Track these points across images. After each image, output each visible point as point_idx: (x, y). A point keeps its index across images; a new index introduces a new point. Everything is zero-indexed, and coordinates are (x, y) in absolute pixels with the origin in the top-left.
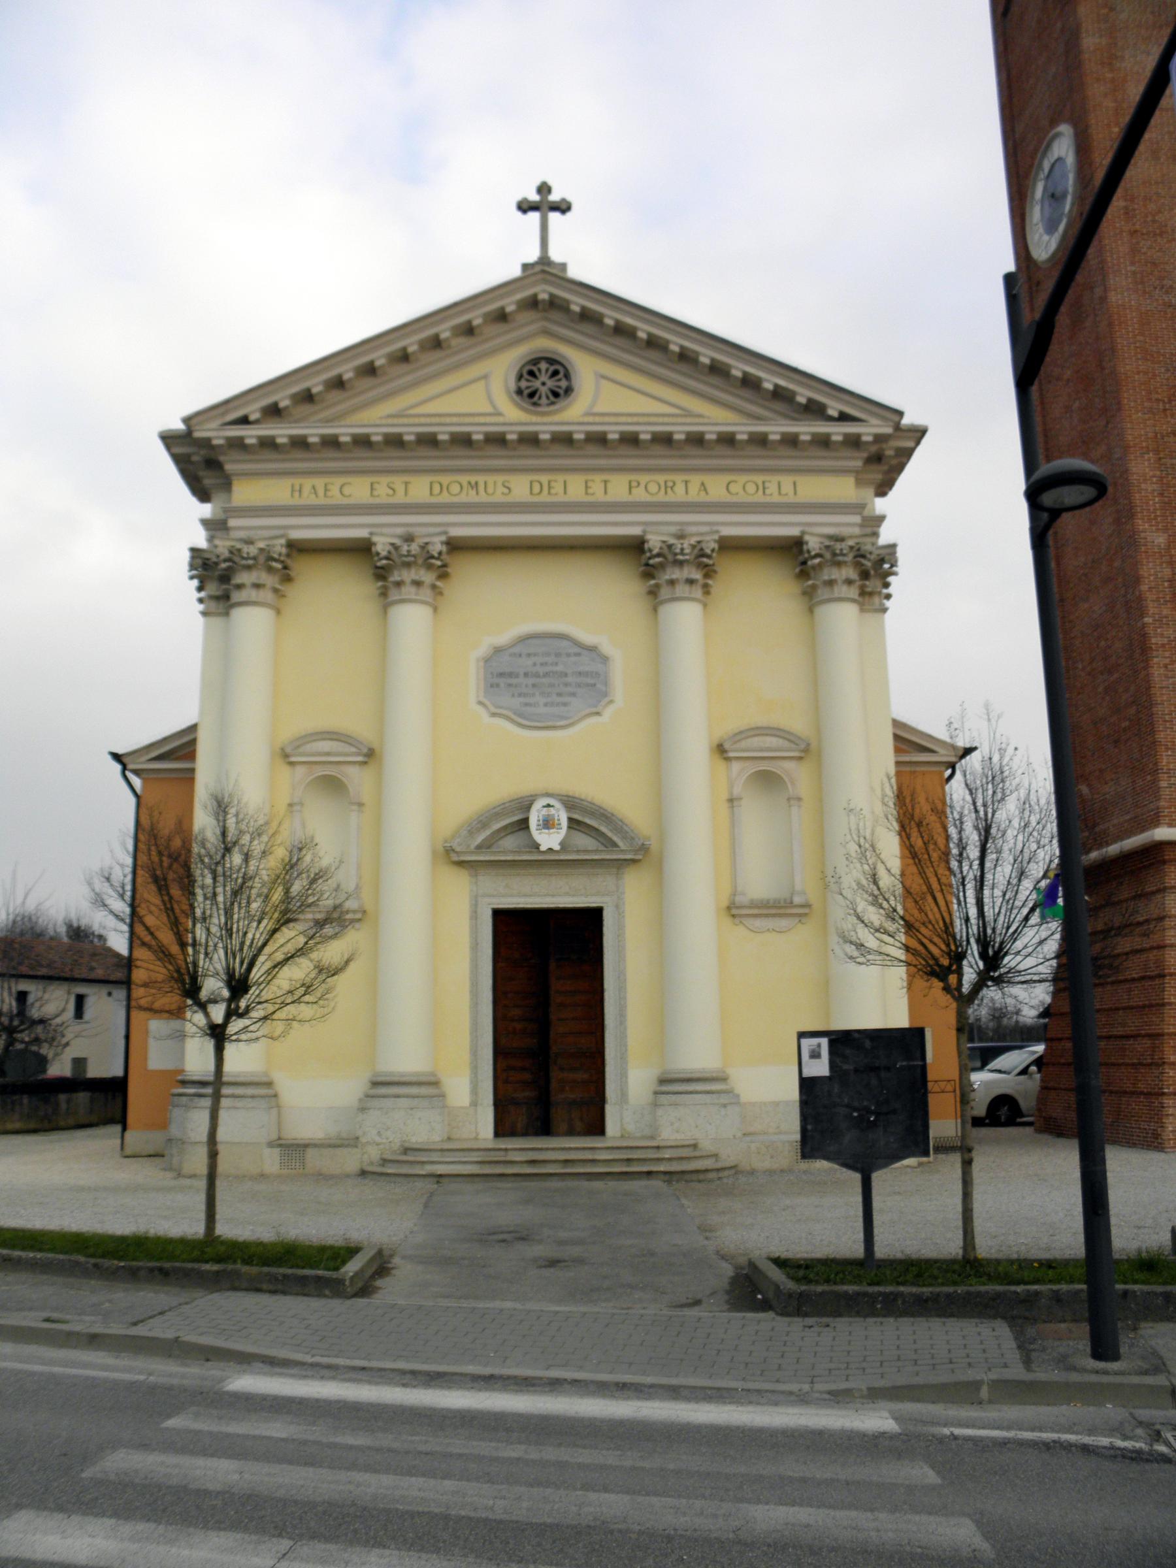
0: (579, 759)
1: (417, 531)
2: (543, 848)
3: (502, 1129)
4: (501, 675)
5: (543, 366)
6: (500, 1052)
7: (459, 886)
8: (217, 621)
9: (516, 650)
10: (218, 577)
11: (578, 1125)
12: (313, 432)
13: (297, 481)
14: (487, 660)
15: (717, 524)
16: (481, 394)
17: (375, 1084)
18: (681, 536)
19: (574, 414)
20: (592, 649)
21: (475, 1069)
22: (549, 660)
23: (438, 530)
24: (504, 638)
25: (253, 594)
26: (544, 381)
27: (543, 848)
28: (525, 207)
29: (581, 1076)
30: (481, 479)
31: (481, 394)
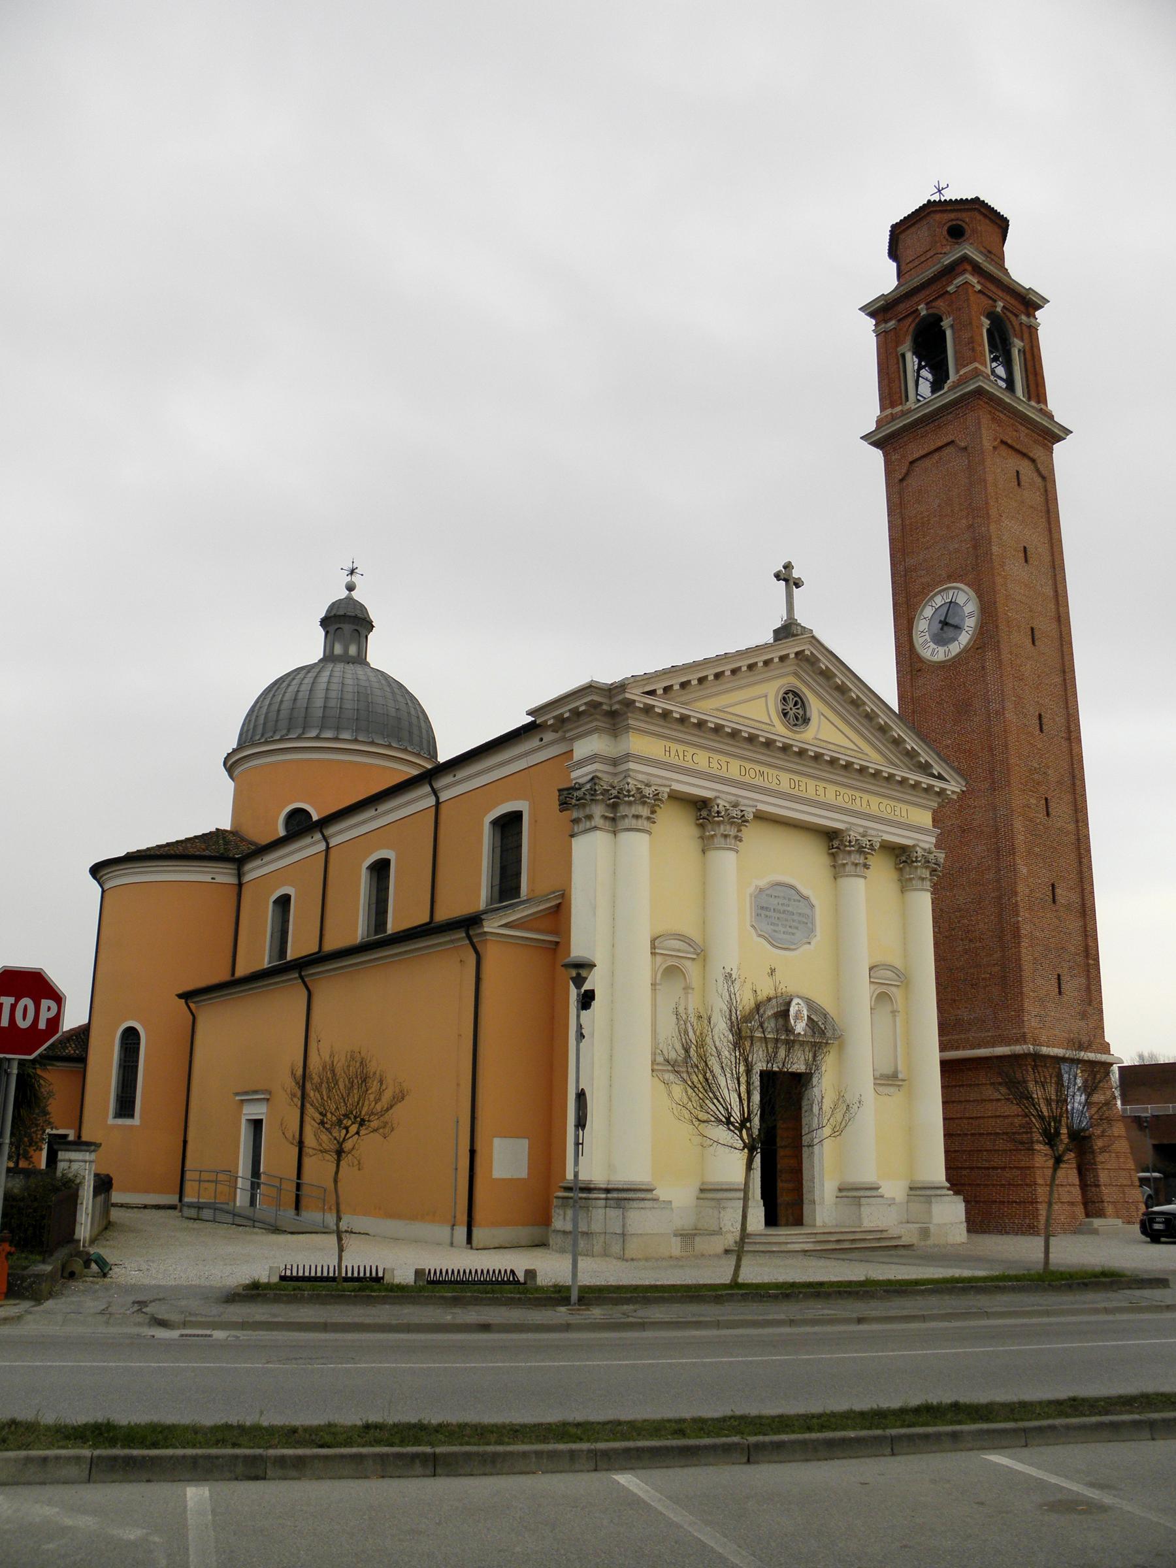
0: (799, 976)
1: (870, 832)
4: (762, 908)
5: (790, 695)
9: (768, 892)
12: (677, 711)
13: (668, 744)
15: (757, 801)
16: (756, 707)
20: (806, 898)
22: (786, 902)
23: (751, 803)
24: (763, 883)
25: (634, 823)
26: (794, 709)
31: (756, 707)
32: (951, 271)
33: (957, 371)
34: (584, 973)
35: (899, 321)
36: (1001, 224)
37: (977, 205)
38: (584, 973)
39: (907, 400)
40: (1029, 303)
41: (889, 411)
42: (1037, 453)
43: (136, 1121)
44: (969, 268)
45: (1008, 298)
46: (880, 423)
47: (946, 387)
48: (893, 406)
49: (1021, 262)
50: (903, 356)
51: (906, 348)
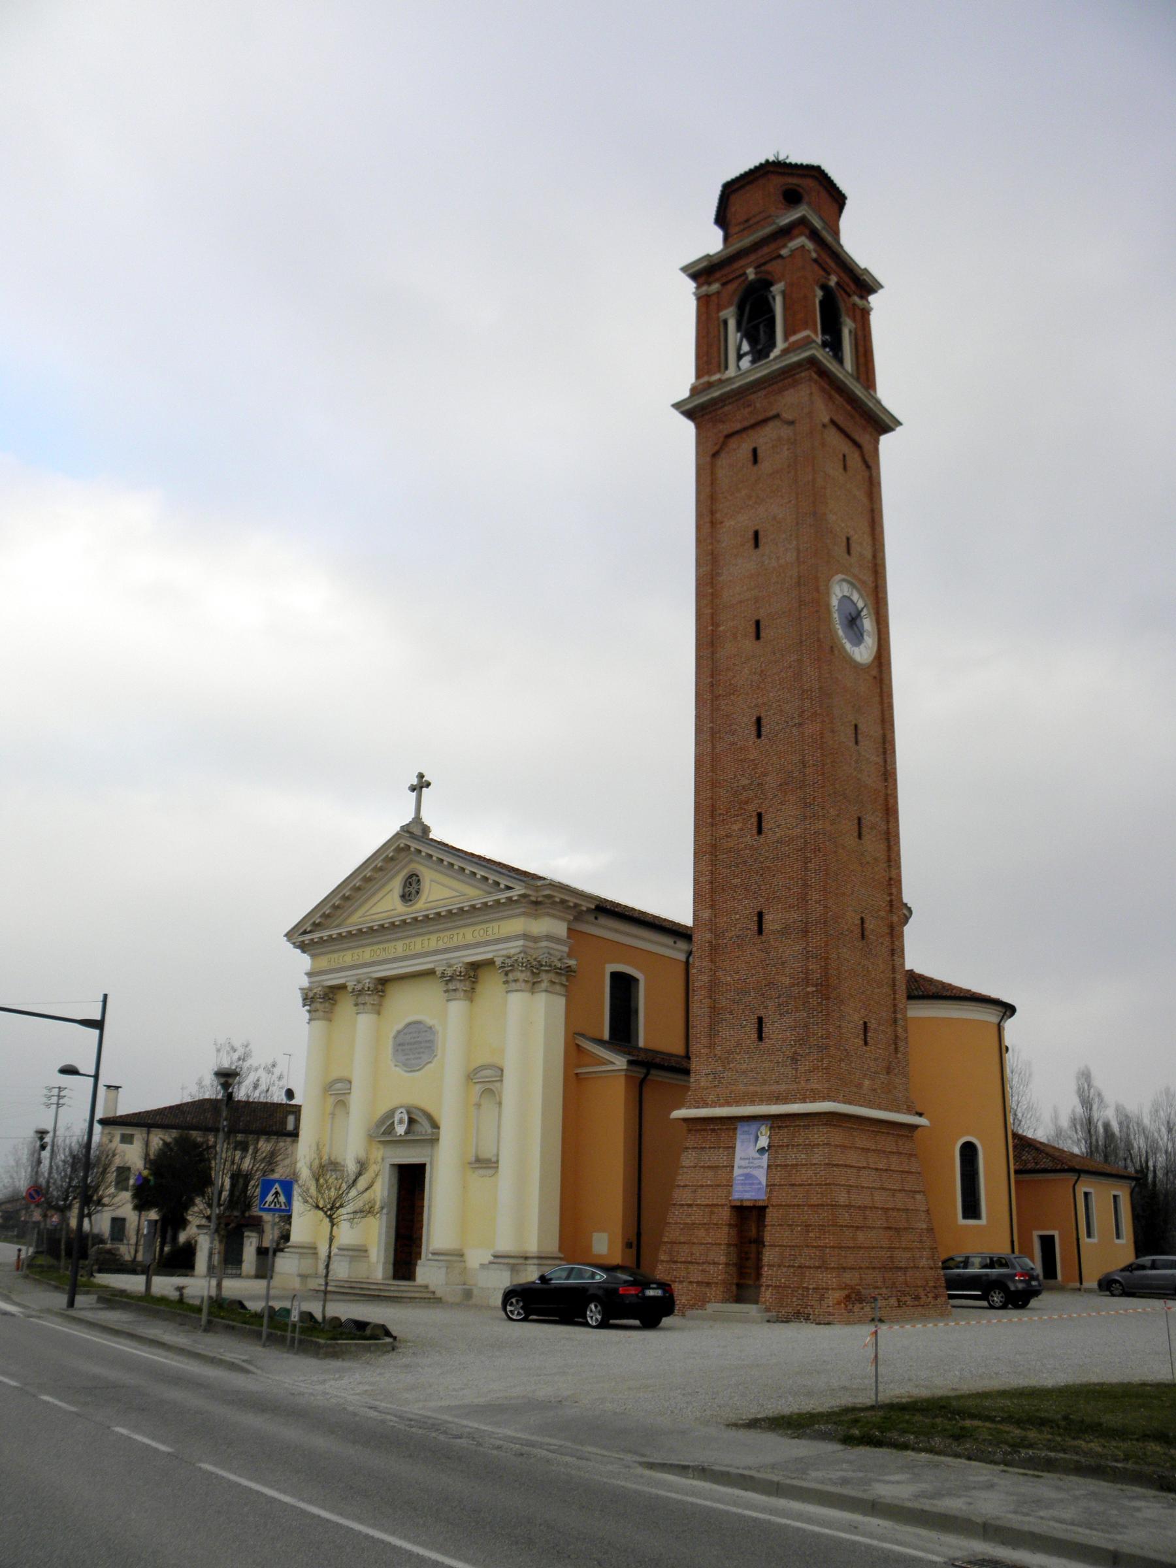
1: (452, 962)
8: (319, 1024)
10: (322, 999)
12: (334, 932)
14: (395, 1037)
17: (496, 1257)
18: (450, 966)
19: (425, 903)
24: (400, 1026)
28: (413, 788)
30: (386, 945)
31: (387, 904)
32: (786, 232)
33: (786, 338)
34: (230, 1081)
35: (724, 284)
36: (839, 199)
37: (816, 174)
38: (230, 1081)
39: (726, 368)
40: (864, 285)
41: (705, 379)
42: (864, 439)
43: (983, 1222)
44: (807, 232)
45: (842, 275)
46: (695, 391)
47: (772, 356)
48: (710, 373)
49: (858, 237)
50: (725, 322)
51: (730, 315)
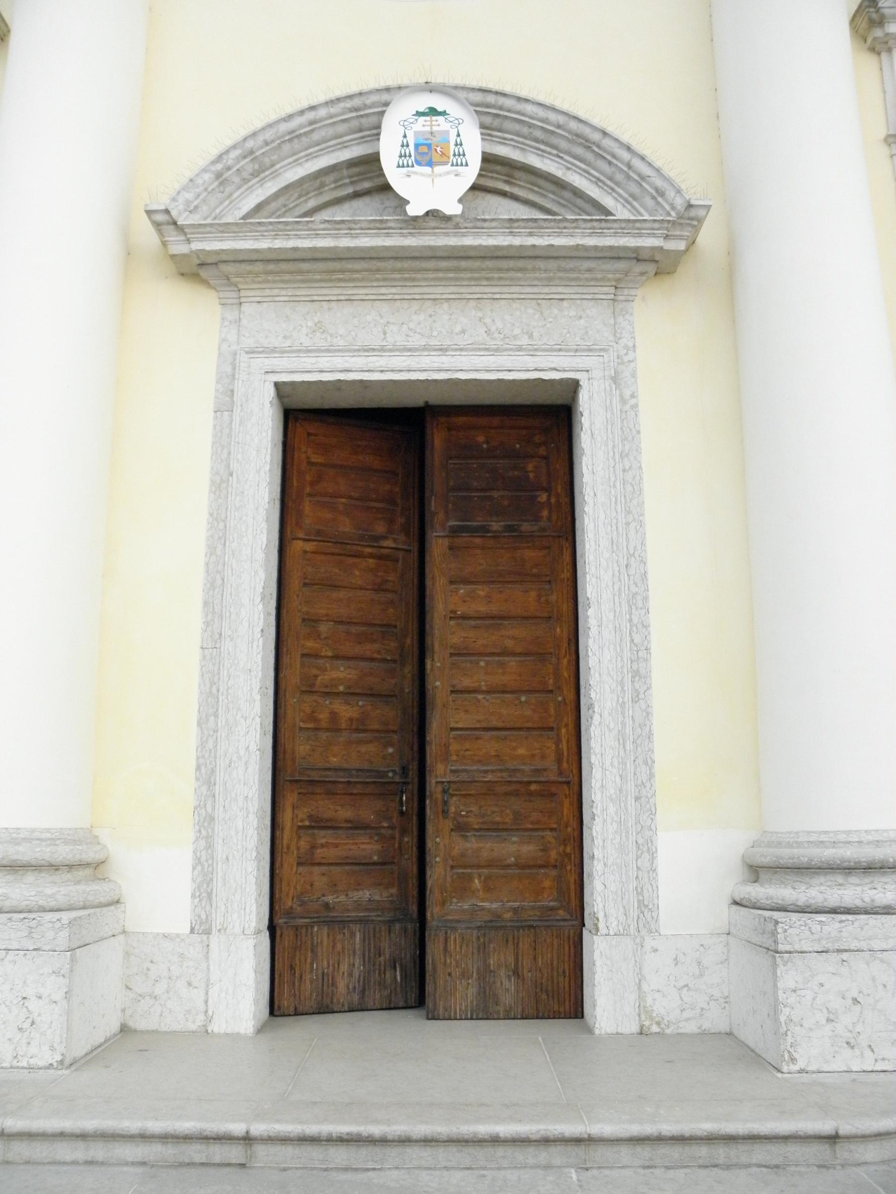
2: (415, 209)
3: (290, 996)
6: (287, 778)
7: (191, 332)
11: (507, 989)
21: (206, 823)
27: (415, 209)
29: (515, 848)
